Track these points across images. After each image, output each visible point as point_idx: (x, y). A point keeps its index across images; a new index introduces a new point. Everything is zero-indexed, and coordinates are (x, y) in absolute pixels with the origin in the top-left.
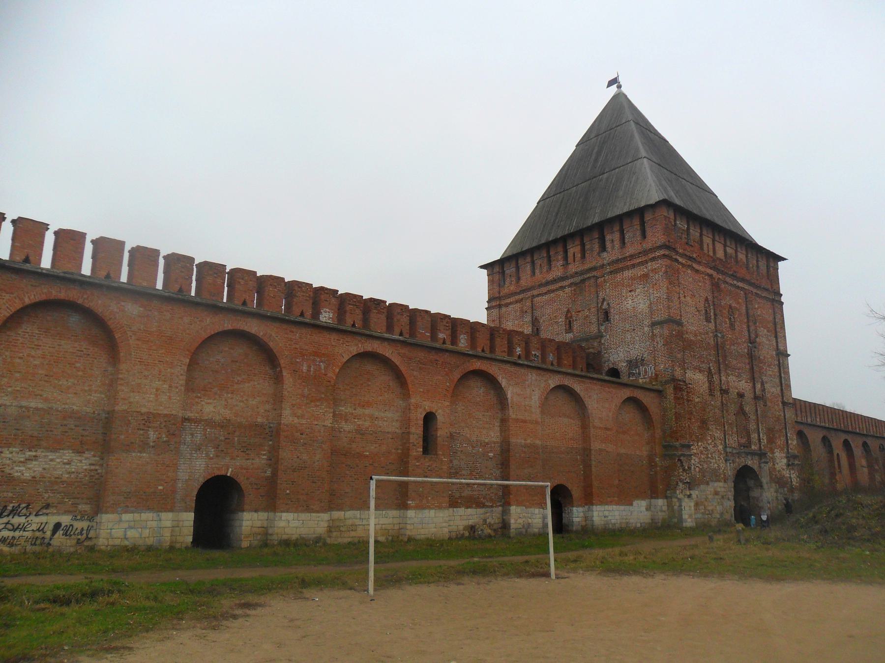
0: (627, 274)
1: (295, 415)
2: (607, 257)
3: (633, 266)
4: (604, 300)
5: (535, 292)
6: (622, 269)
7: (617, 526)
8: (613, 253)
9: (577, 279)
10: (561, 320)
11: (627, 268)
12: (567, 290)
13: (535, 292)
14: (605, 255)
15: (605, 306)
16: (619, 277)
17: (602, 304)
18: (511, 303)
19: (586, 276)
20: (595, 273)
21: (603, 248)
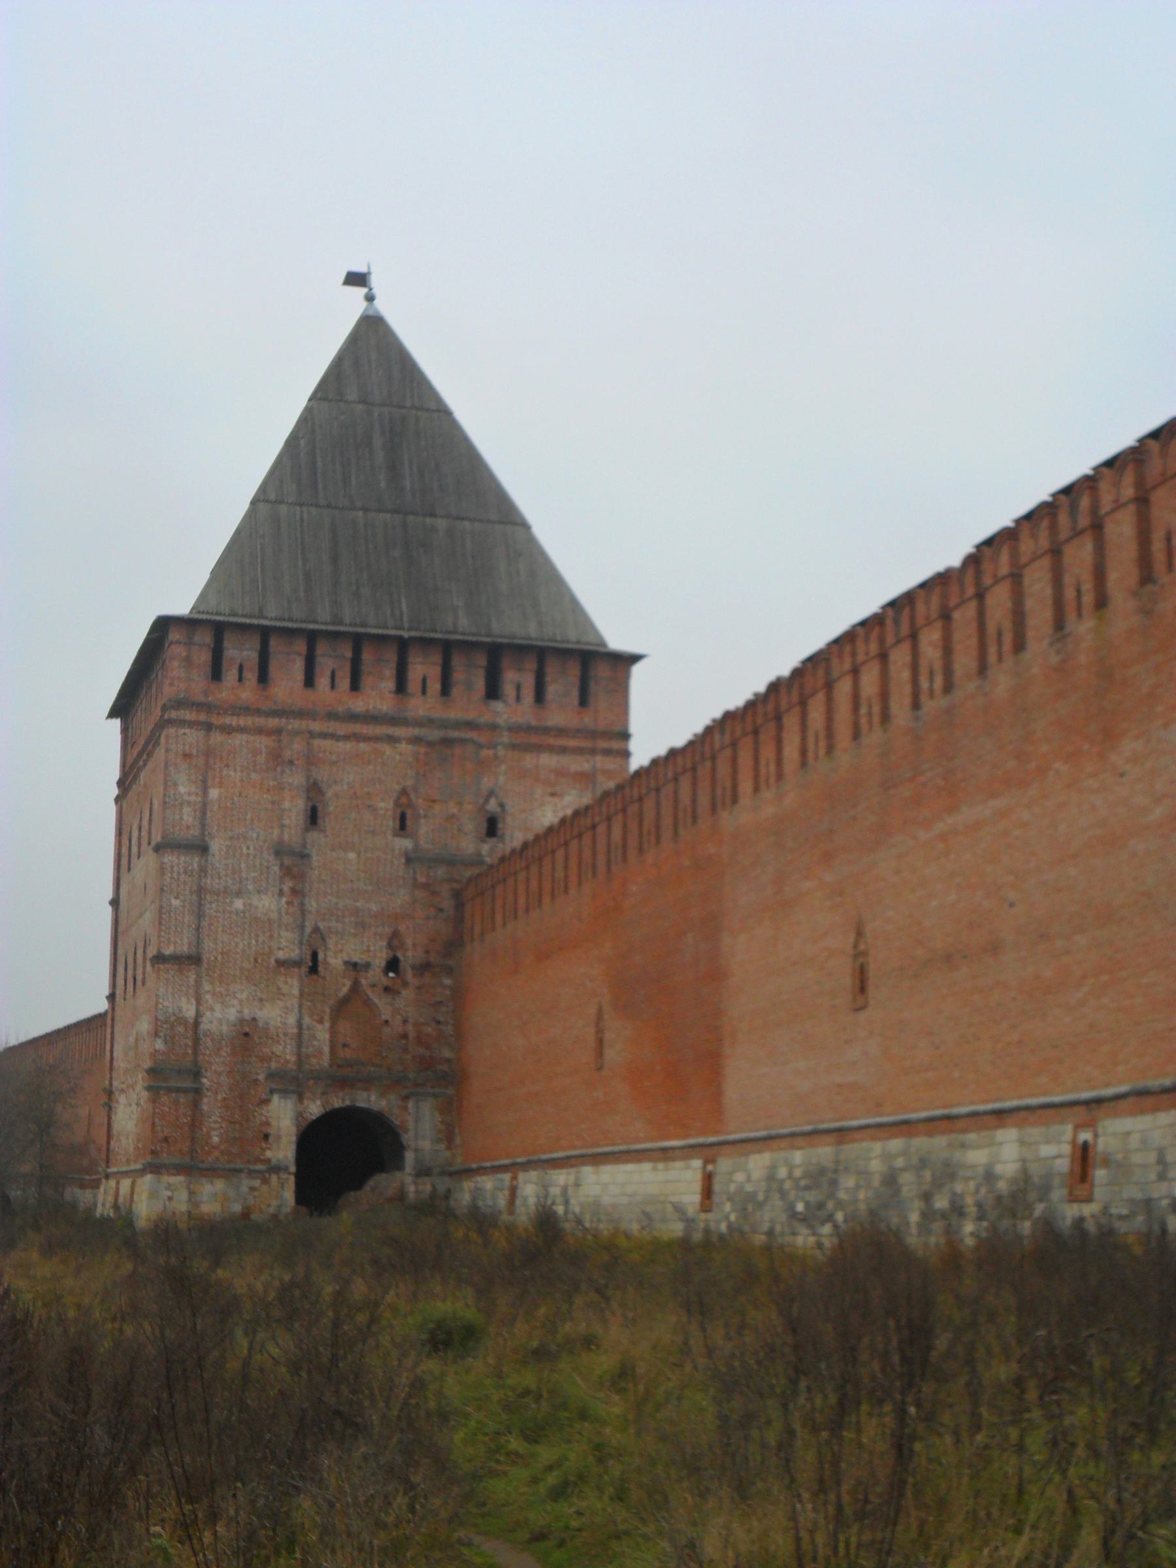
0: (548, 761)
1: (502, 1180)
2: (502, 712)
3: (563, 750)
4: (491, 794)
5: (316, 726)
6: (539, 748)
7: (801, 1252)
8: (378, 695)
9: (435, 734)
10: (386, 805)
11: (551, 749)
12: (403, 747)
13: (316, 726)
14: (498, 706)
15: (492, 806)
16: (529, 760)
17: (487, 800)
18: (242, 730)
19: (455, 734)
20: (473, 735)
21: (493, 692)
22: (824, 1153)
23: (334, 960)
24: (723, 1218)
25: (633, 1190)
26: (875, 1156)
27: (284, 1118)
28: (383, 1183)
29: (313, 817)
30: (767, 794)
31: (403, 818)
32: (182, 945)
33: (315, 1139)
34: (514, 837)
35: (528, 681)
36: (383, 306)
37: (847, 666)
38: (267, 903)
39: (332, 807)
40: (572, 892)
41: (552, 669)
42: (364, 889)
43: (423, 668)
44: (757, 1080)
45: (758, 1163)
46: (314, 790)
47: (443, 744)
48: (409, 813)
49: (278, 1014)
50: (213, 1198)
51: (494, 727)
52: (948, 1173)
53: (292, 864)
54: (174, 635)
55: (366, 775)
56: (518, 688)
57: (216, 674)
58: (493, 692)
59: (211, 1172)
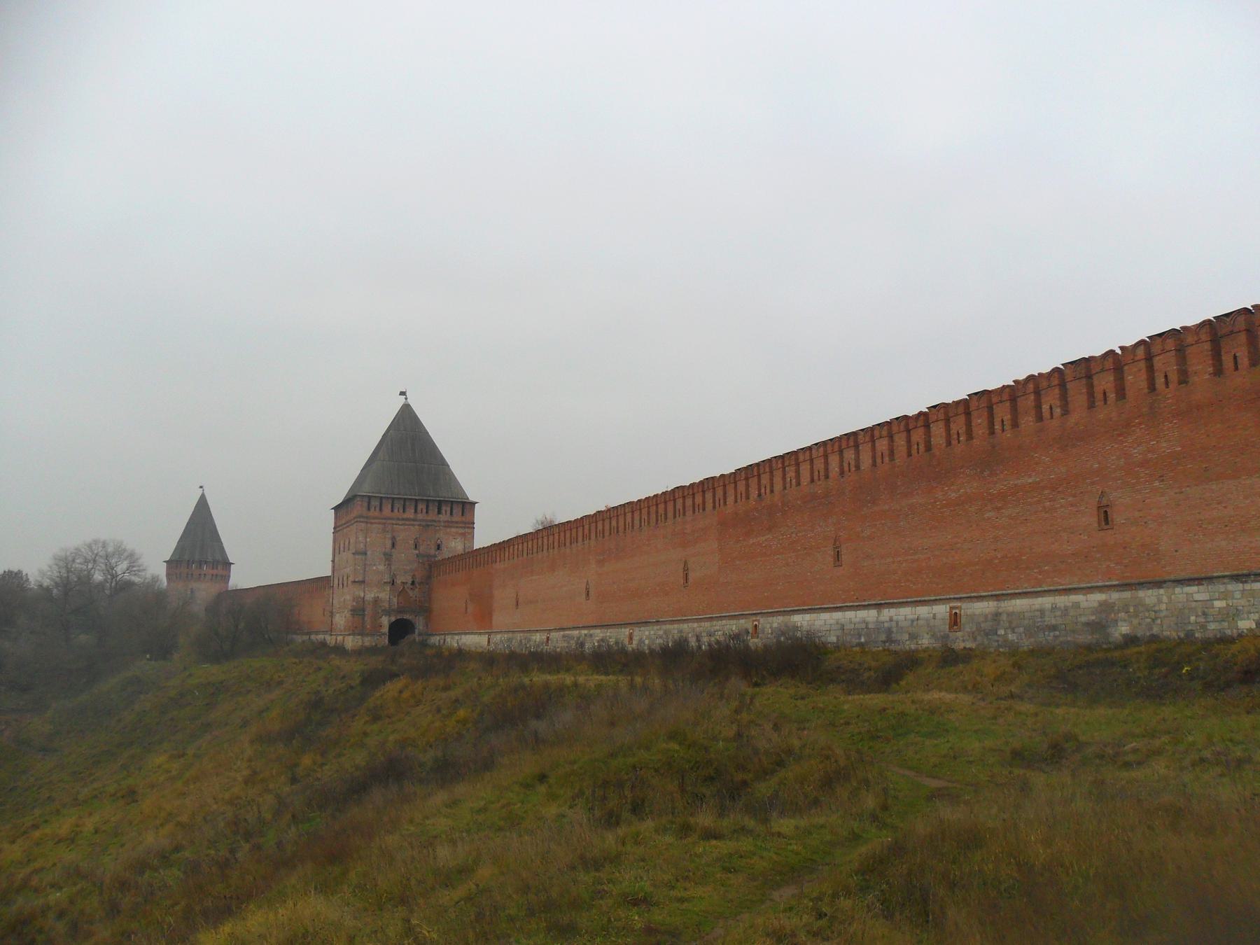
2: (443, 517)
8: (410, 513)
21: (439, 512)
22: (510, 635)
23: (398, 581)
24: (492, 647)
25: (474, 641)
26: (519, 636)
27: (385, 621)
28: (409, 638)
29: (393, 545)
32: (361, 579)
33: (393, 626)
35: (449, 509)
36: (409, 401)
38: (381, 568)
41: (455, 506)
42: (406, 564)
43: (421, 506)
44: (499, 619)
45: (499, 636)
46: (393, 538)
47: (426, 526)
49: (384, 595)
50: (368, 641)
52: (529, 640)
53: (388, 557)
55: (407, 534)
57: (369, 509)
58: (439, 512)
59: (367, 635)
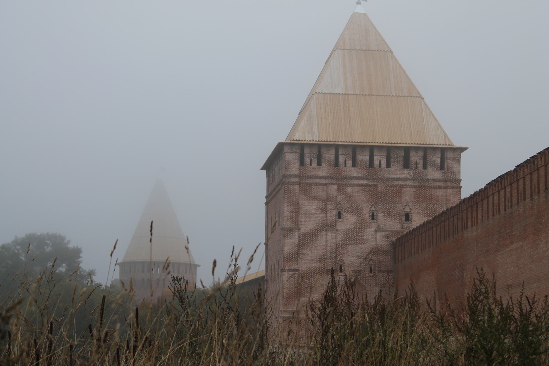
21: (407, 165)
30: (474, 228)
31: (373, 215)
34: (417, 221)
37: (491, 193)
39: (344, 214)
40: (427, 249)
48: (375, 213)
51: (407, 179)
54: (286, 149)
56: (416, 163)
